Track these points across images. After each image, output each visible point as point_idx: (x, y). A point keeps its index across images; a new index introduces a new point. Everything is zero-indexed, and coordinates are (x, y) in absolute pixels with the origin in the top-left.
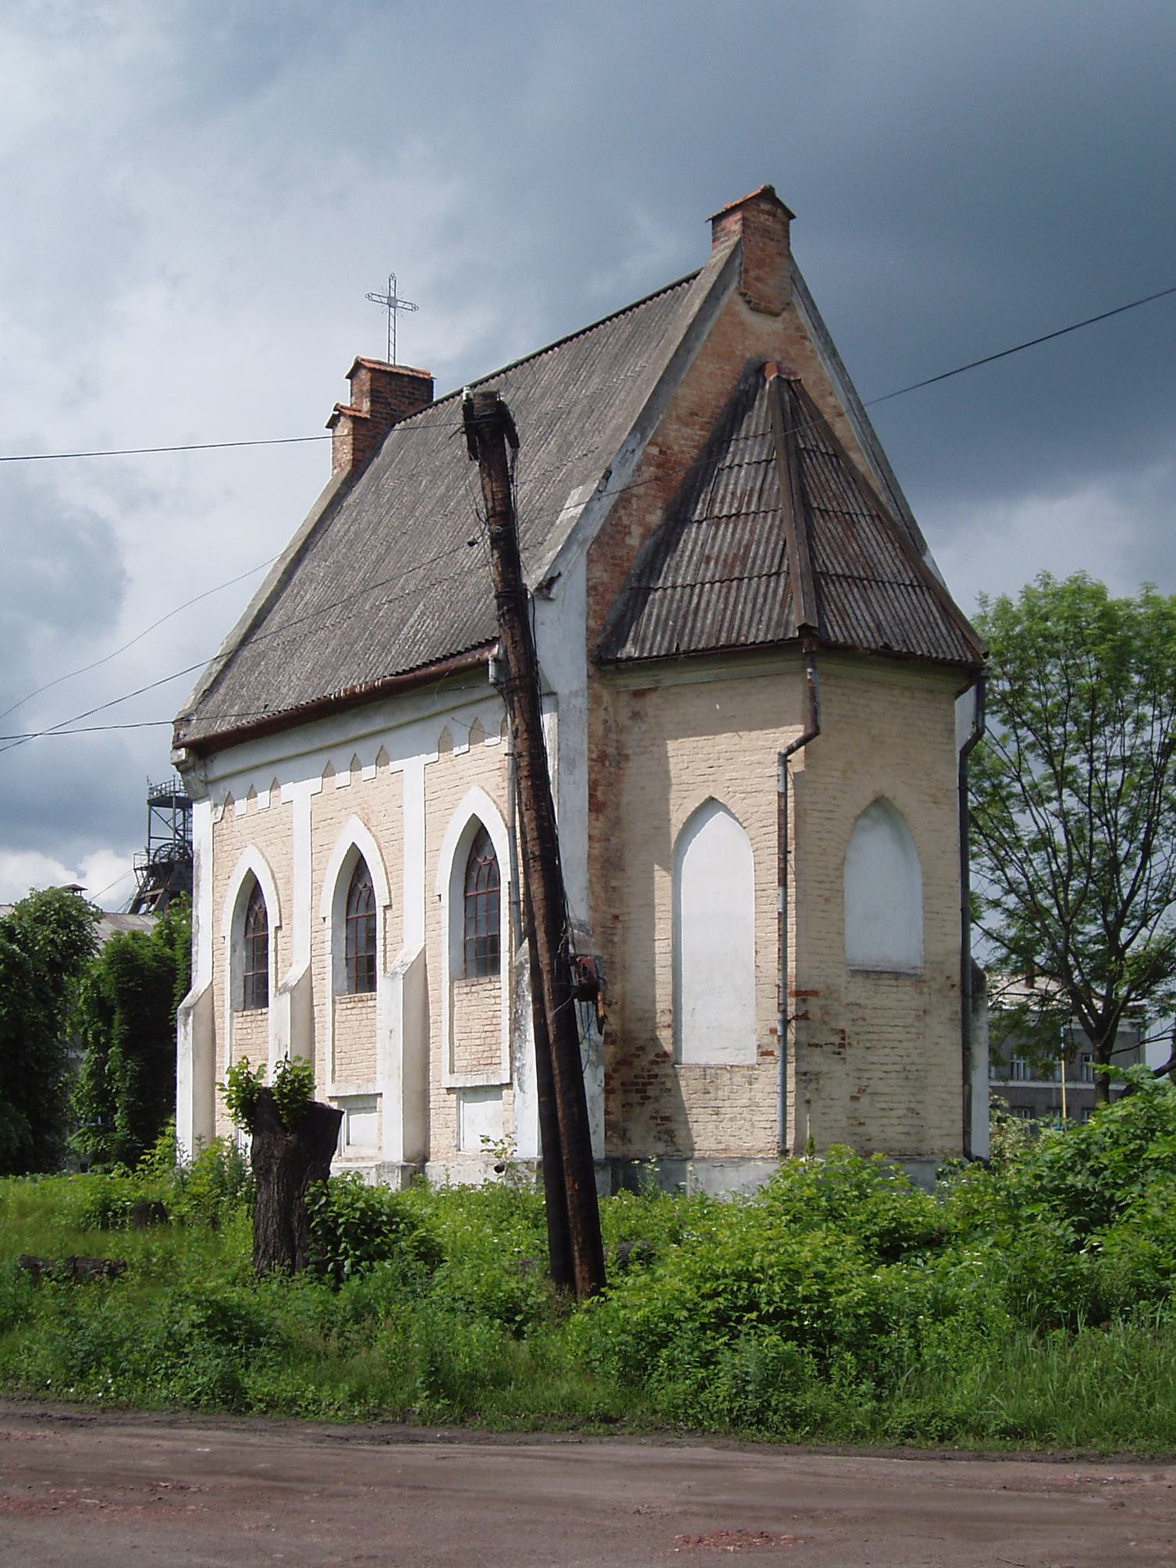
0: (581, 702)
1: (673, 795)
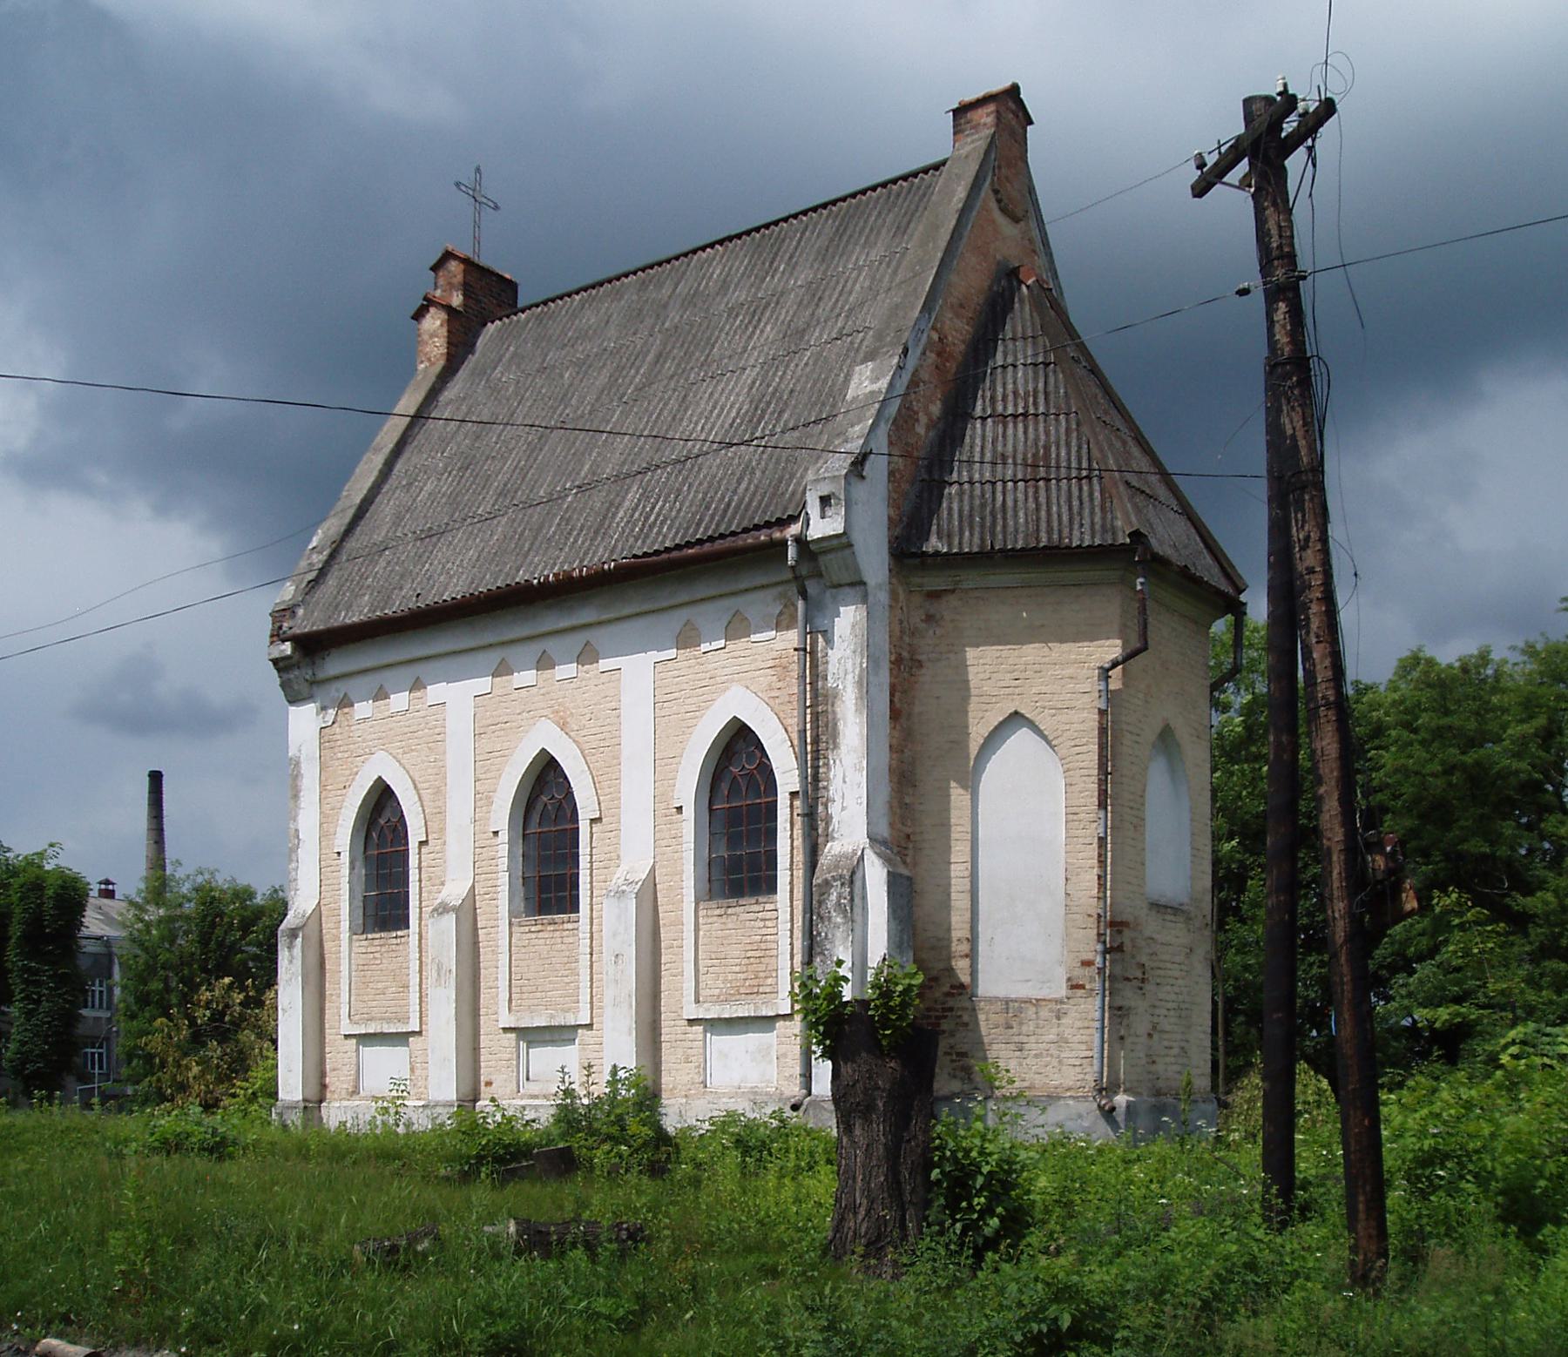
0: (883, 597)
1: (972, 707)
